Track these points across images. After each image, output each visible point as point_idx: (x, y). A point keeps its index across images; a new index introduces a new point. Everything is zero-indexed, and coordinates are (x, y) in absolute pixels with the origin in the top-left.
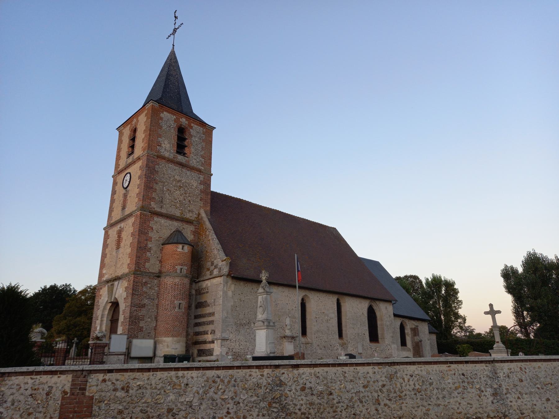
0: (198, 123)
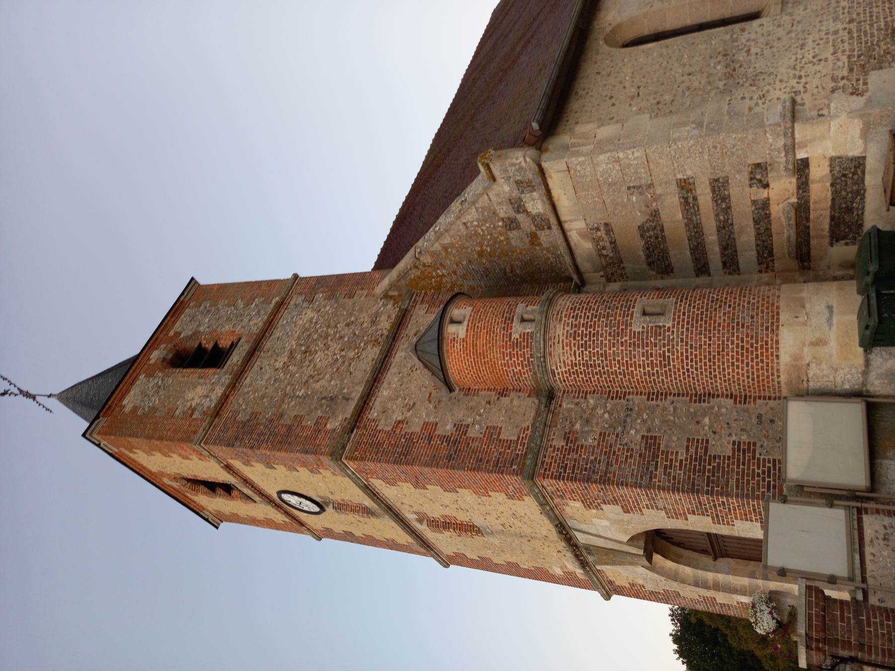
0: (173, 319)
